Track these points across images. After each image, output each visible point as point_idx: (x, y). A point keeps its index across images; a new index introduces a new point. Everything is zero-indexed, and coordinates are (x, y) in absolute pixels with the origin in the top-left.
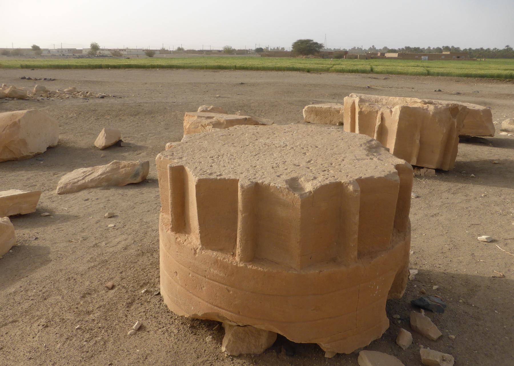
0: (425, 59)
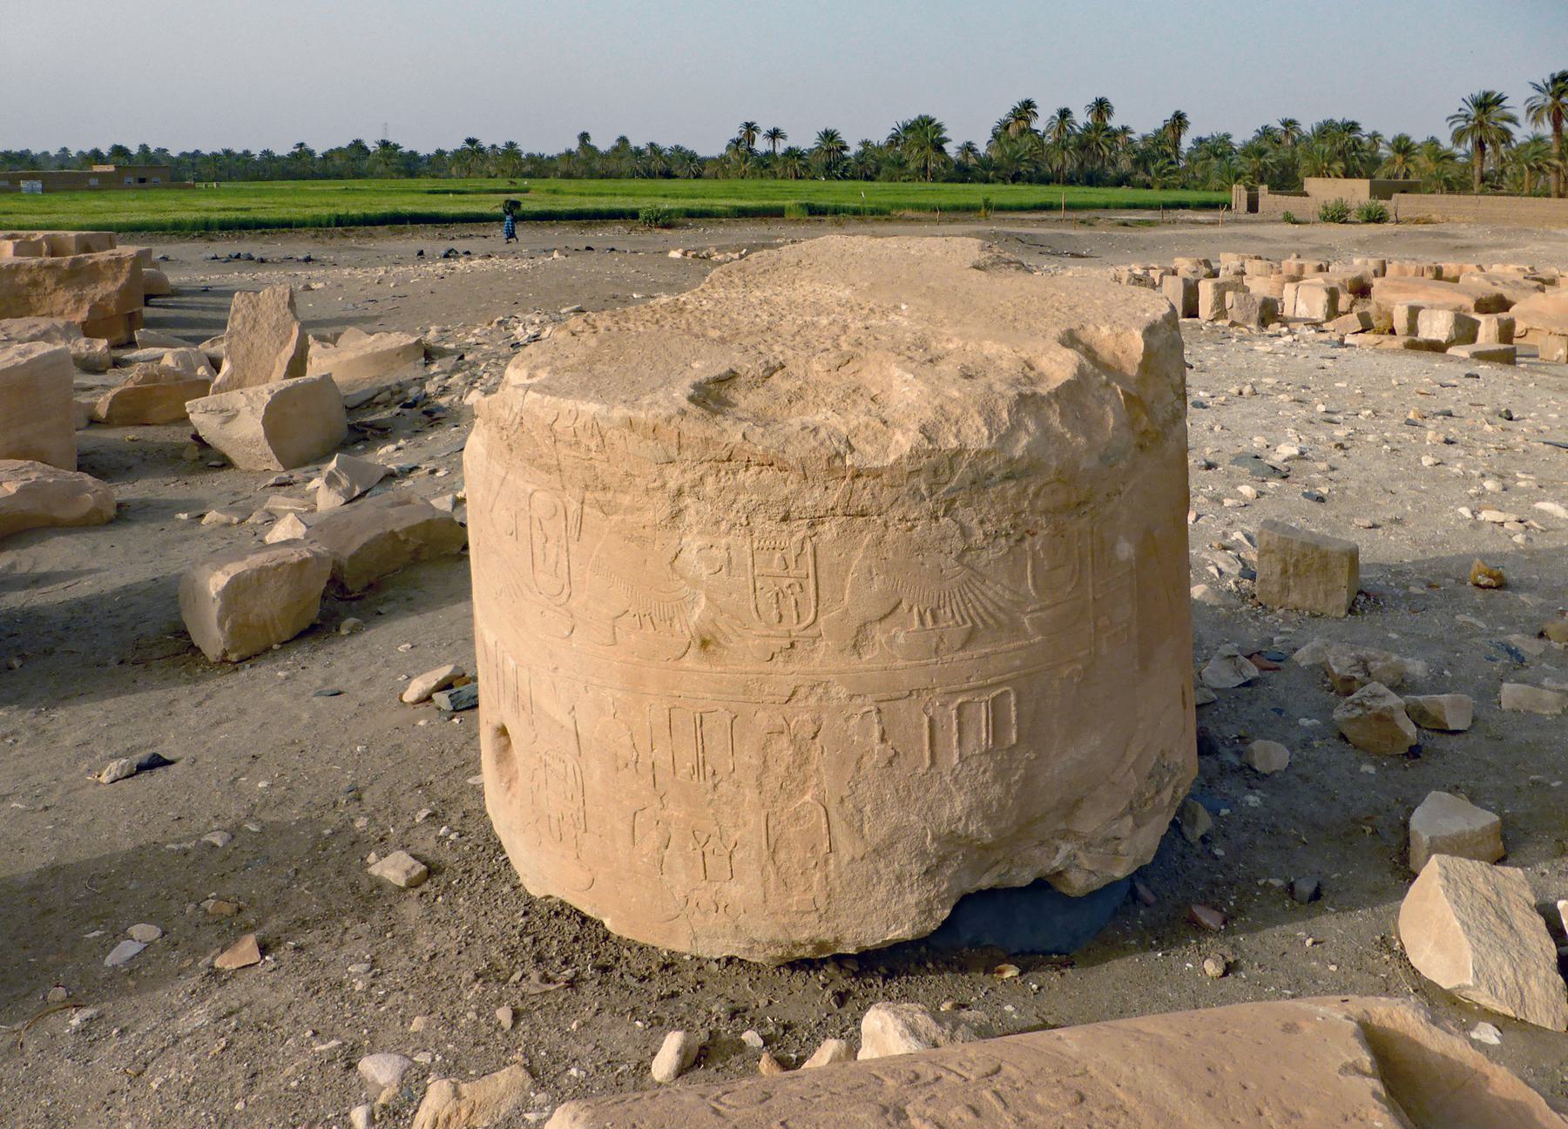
0: (32, 190)
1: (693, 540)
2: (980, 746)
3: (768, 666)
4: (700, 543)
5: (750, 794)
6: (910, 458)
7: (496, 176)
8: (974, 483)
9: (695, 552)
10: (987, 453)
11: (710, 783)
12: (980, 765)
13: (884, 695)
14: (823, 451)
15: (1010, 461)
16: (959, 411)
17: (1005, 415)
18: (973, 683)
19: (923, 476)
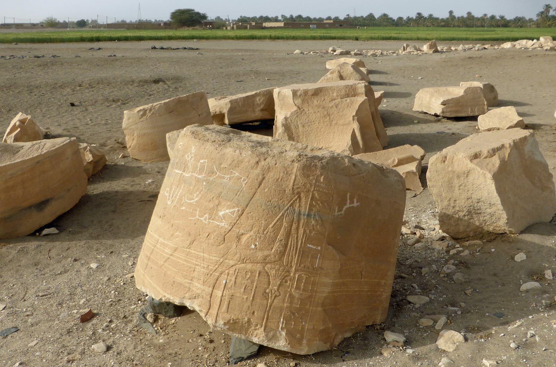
7: (430, 26)
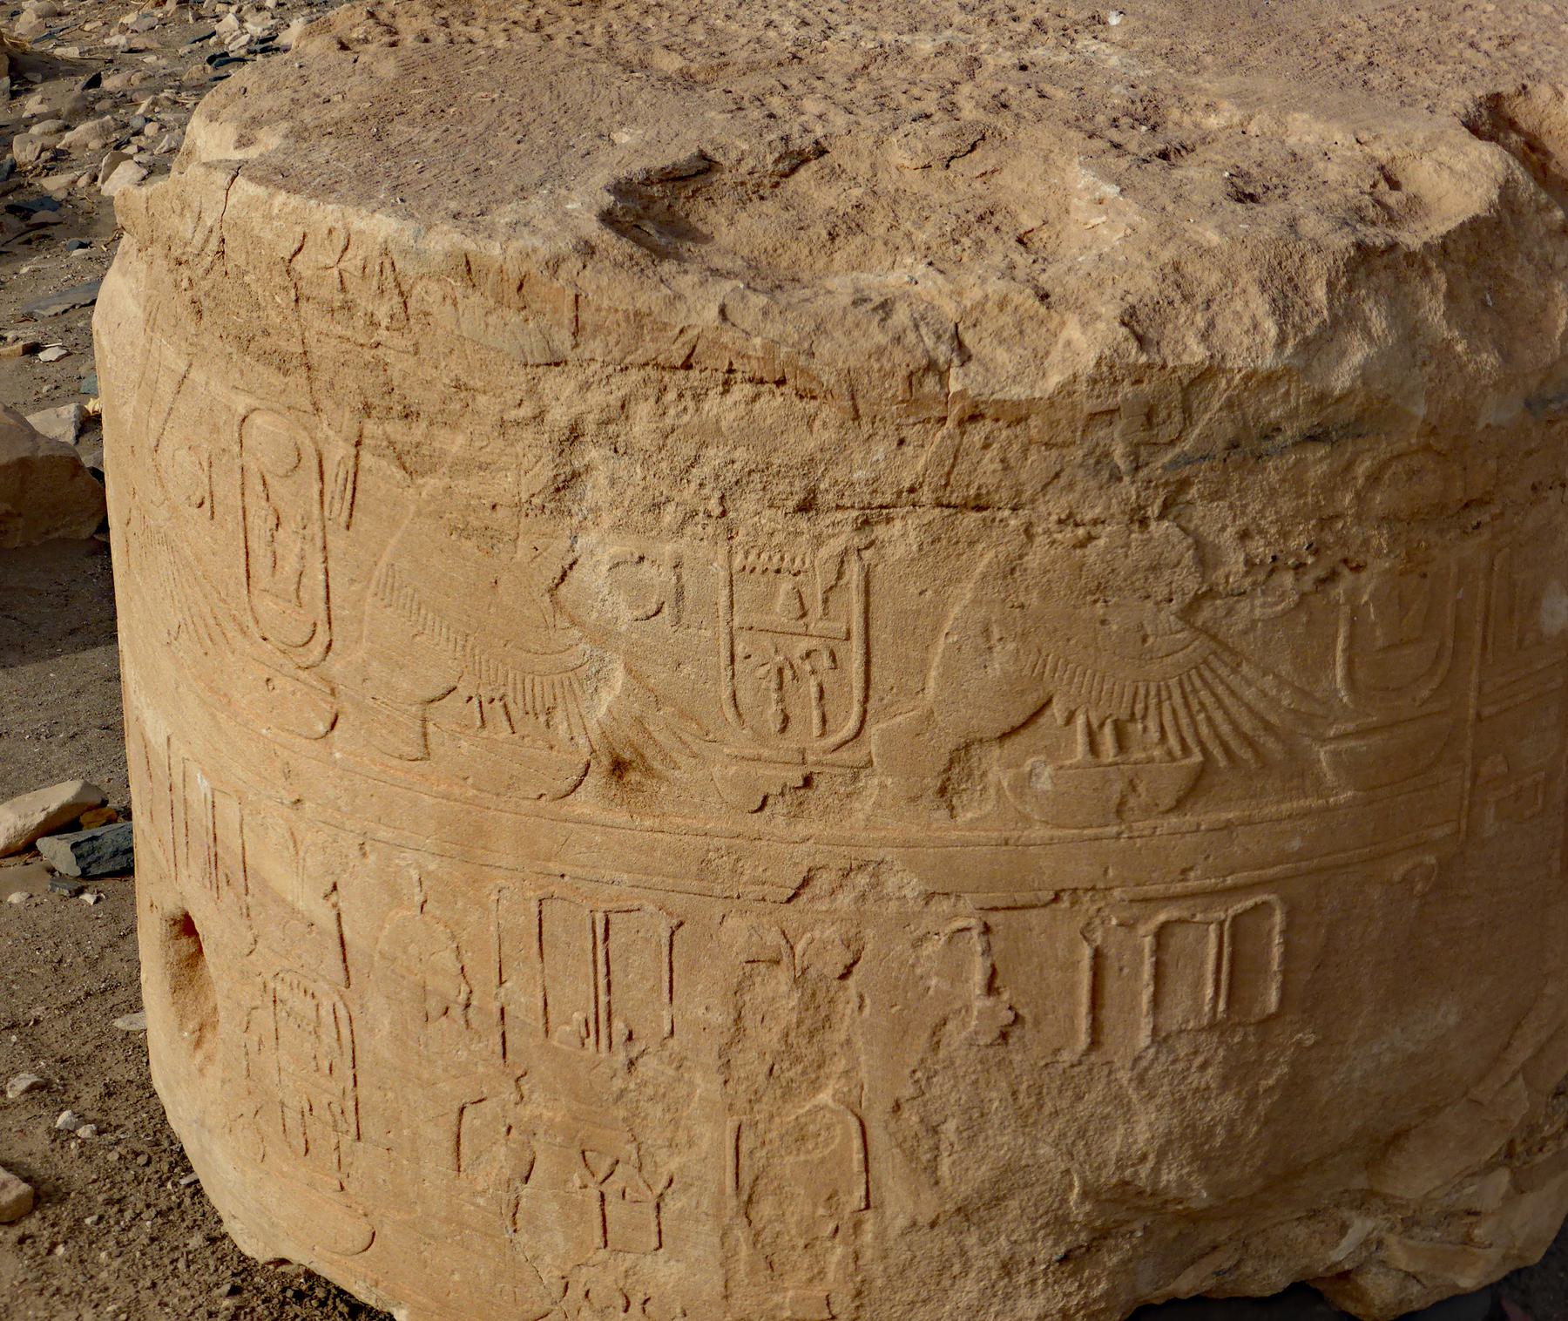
1: (601, 542)
2: (1197, 1011)
3: (757, 823)
4: (614, 550)
5: (705, 1085)
6: (1093, 381)
8: (1234, 445)
9: (604, 568)
10: (1270, 379)
11: (621, 1057)
12: (1196, 1053)
13: (998, 898)
14: (898, 356)
15: (1321, 399)
16: (1214, 278)
17: (1320, 293)
18: (1193, 883)
19: (1120, 424)
